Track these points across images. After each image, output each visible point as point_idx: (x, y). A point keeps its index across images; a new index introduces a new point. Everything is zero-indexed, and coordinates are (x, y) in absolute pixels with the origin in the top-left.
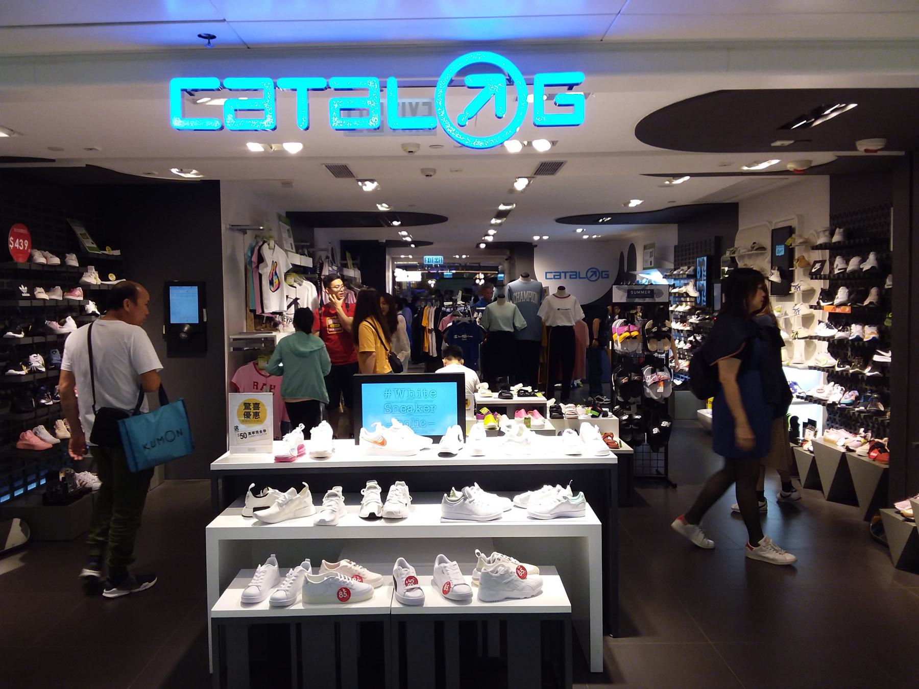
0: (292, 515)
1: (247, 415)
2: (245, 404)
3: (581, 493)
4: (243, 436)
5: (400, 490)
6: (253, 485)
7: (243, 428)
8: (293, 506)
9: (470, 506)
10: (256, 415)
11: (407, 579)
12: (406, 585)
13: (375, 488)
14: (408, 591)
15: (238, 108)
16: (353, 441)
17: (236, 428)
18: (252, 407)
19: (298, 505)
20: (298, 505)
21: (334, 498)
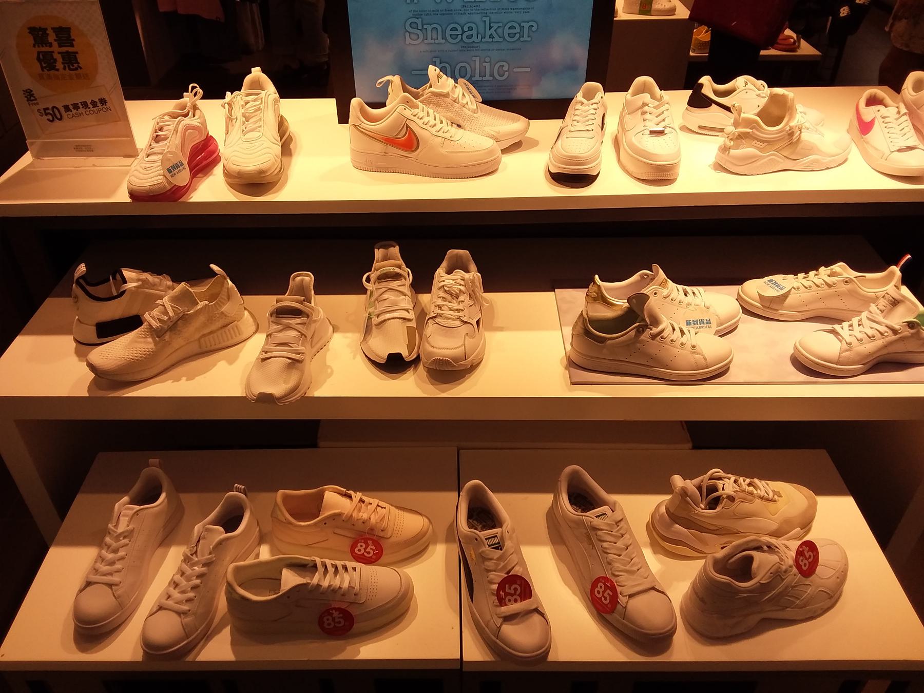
0: (194, 348)
1: (46, 61)
2: (32, 30)
3: (700, 81)
4: (53, 115)
5: (455, 279)
6: (82, 268)
7: (48, 96)
8: (191, 331)
9: (653, 348)
10: (71, 60)
11: (502, 585)
12: (502, 602)
13: (397, 276)
14: (508, 619)
15: (691, 319)
16: (329, 106)
17: (29, 95)
18: (52, 37)
19: (205, 325)
20: (205, 325)
21: (294, 321)
